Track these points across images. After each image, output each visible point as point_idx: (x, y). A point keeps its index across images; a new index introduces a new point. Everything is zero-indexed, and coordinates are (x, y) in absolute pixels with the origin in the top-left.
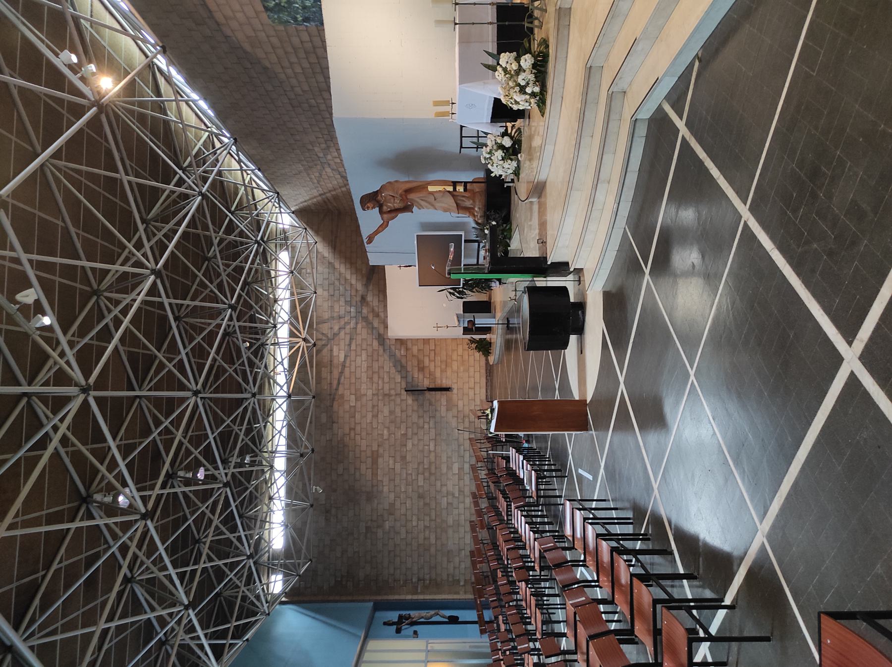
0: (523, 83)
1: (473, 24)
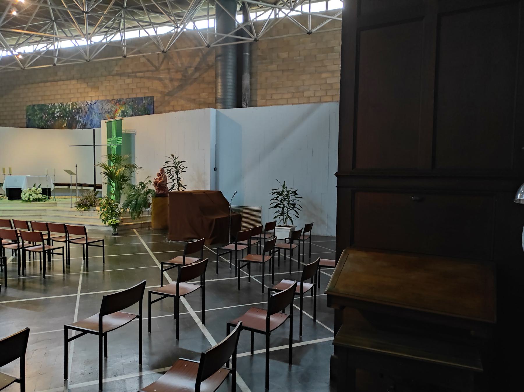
0: (33, 195)
1: (47, 180)
